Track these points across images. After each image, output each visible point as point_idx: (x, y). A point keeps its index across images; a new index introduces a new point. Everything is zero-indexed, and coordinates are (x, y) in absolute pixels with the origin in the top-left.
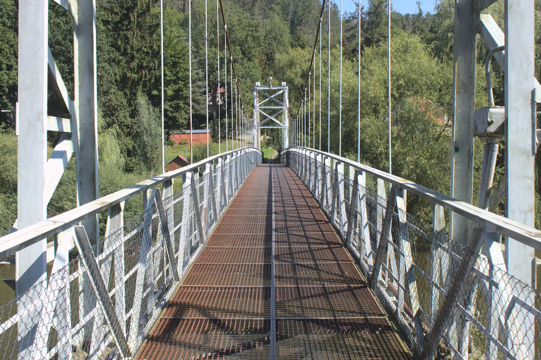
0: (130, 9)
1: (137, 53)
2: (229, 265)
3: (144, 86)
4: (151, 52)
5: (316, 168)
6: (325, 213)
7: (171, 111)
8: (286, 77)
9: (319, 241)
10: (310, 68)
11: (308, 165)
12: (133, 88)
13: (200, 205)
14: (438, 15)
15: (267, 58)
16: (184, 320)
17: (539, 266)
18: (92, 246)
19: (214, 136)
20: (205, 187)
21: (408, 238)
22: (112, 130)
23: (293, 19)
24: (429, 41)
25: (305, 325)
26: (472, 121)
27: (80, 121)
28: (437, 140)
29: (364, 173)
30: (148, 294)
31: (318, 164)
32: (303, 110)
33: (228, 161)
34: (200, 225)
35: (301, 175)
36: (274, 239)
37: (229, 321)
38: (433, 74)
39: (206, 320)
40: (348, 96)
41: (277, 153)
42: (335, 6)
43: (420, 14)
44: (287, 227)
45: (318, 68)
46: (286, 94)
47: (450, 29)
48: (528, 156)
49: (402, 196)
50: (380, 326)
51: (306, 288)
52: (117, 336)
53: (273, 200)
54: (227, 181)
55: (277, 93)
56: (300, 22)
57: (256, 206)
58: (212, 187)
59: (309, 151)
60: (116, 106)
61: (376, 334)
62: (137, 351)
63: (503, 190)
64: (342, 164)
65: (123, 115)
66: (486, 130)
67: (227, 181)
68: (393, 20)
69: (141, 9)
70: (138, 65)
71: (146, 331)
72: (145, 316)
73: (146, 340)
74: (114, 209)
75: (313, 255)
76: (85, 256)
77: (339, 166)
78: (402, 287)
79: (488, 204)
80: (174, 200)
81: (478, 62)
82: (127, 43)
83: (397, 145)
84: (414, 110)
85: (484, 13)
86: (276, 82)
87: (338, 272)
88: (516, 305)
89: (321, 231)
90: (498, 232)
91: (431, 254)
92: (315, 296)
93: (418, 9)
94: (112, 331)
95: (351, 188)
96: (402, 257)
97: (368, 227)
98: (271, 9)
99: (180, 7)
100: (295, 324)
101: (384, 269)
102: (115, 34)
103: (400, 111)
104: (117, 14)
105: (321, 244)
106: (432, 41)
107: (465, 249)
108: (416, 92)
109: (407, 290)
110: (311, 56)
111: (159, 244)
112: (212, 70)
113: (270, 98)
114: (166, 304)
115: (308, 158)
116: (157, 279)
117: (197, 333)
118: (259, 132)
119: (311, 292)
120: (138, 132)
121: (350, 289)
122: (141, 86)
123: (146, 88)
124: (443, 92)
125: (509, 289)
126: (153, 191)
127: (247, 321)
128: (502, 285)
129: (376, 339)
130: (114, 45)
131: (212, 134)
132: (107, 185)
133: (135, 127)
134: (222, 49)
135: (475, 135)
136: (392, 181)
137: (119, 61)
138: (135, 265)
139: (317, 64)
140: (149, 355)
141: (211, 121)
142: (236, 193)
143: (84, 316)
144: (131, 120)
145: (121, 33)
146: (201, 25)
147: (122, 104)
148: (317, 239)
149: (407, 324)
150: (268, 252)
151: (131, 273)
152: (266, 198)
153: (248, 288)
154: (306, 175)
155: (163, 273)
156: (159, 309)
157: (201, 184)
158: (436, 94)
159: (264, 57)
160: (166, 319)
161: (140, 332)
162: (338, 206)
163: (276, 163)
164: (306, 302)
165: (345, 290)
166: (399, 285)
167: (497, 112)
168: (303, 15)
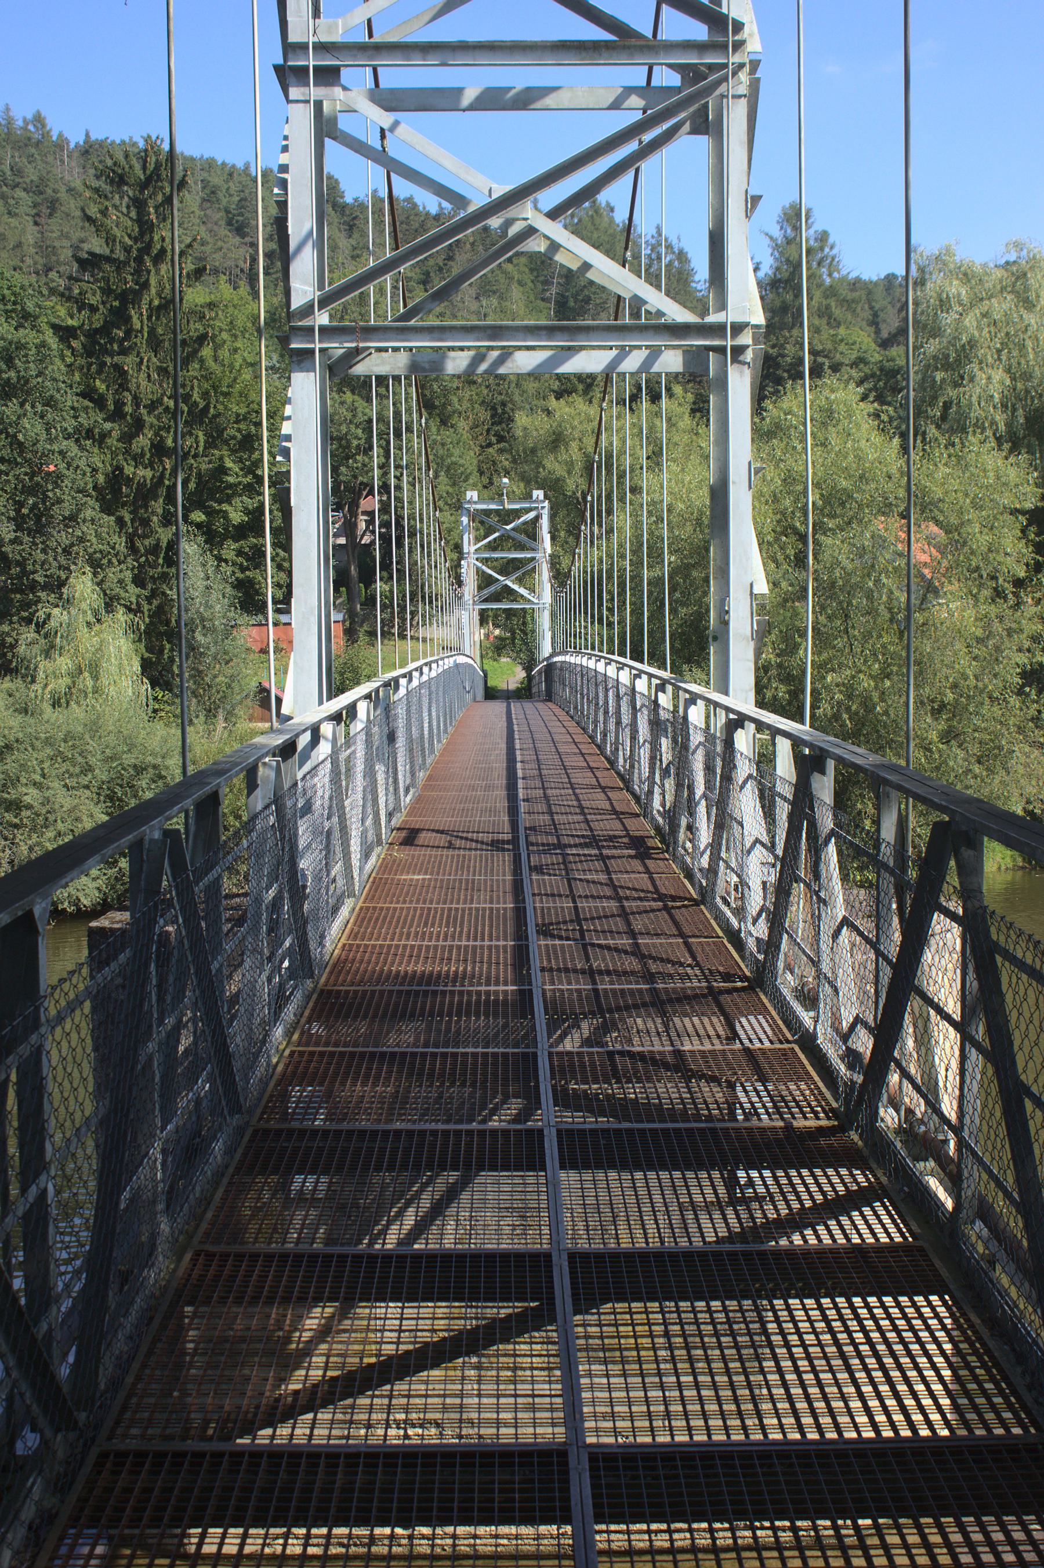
0: (129, 298)
1: (149, 413)
4: (186, 409)
5: (635, 710)
8: (543, 473)
12: (141, 507)
15: (492, 417)
20: (358, 755)
23: (563, 296)
41: (523, 674)
46: (545, 523)
55: (522, 520)
59: (627, 669)
60: (98, 555)
82: (124, 387)
86: (519, 488)
99: (241, 264)
102: (91, 364)
104: (93, 309)
113: (502, 532)
115: (600, 678)
118: (477, 618)
122: (161, 500)
131: (347, 624)
132: (120, 749)
137: (104, 435)
141: (343, 589)
144: (138, 590)
145: (108, 360)
147: (113, 548)
159: (484, 415)
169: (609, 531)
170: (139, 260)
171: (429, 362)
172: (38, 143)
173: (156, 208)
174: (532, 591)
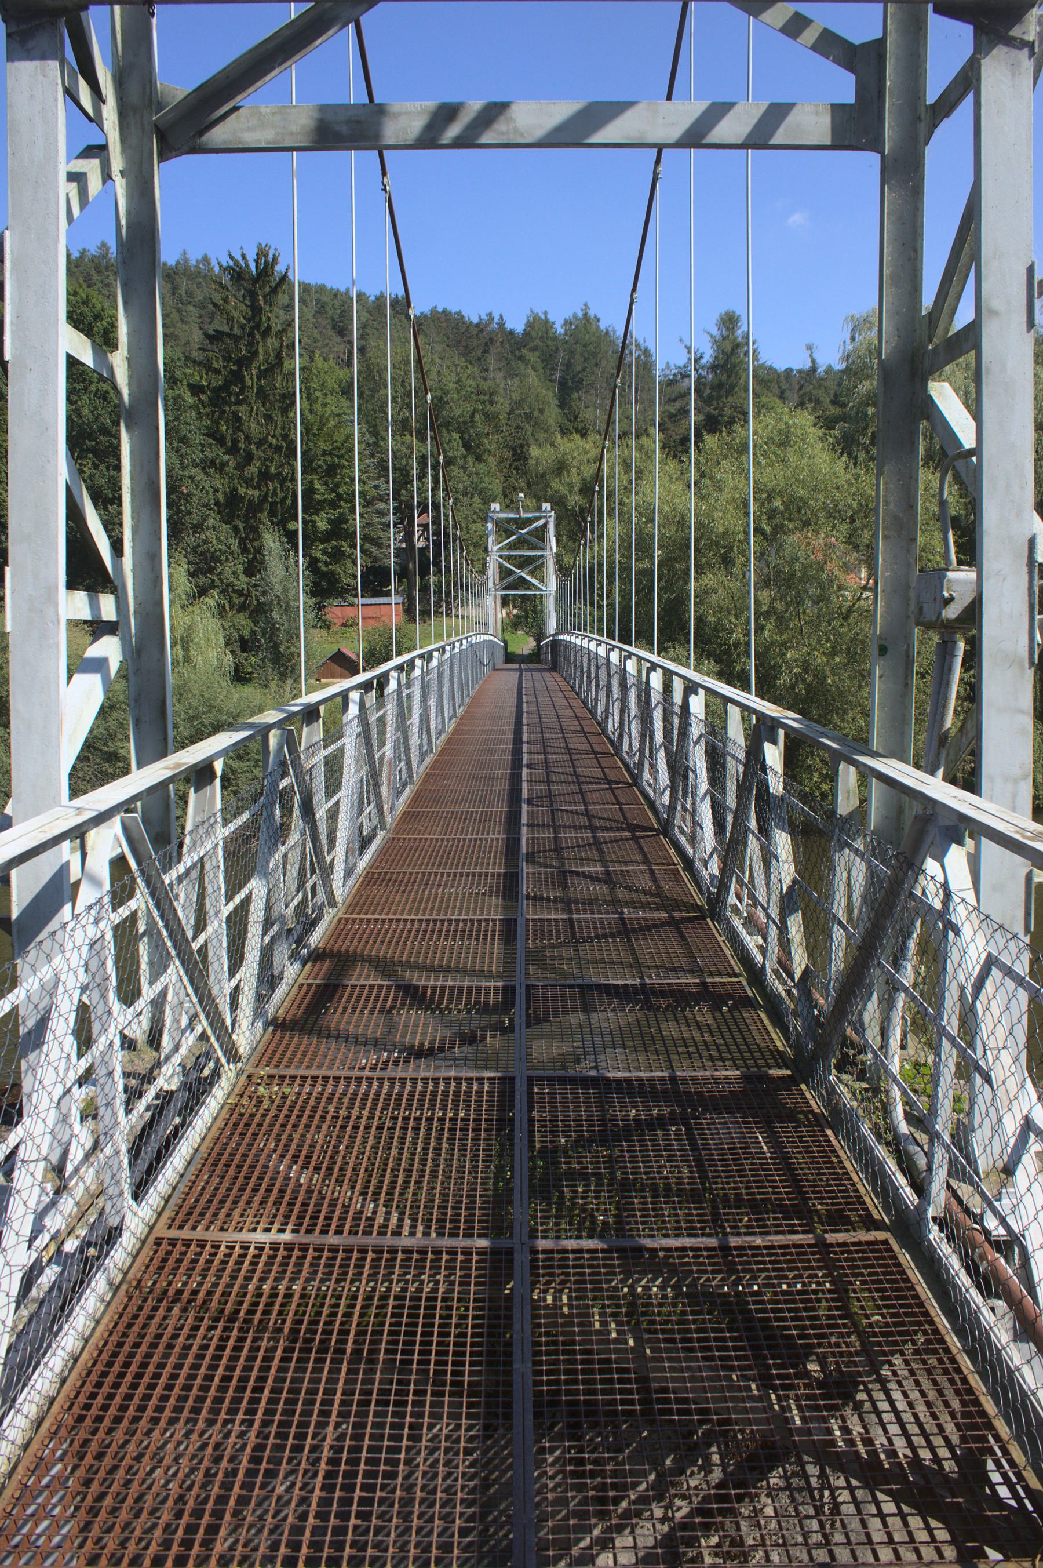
0: (244, 363)
2: (436, 874)
3: (272, 513)
5: (609, 676)
6: (626, 766)
7: (326, 562)
8: (550, 492)
9: (614, 825)
10: (598, 477)
11: (593, 670)
13: (377, 756)
14: (847, 371)
16: (346, 986)
17: (1040, 885)
18: (156, 853)
19: (409, 611)
20: (389, 718)
21: (786, 826)
22: (211, 600)
24: (828, 423)
25: (583, 996)
26: (912, 594)
27: (135, 597)
28: (846, 618)
29: (701, 691)
30: (273, 937)
31: (613, 669)
32: (585, 557)
33: (435, 663)
34: (378, 795)
35: (580, 687)
36: (524, 820)
37: (434, 988)
38: (838, 488)
39: (389, 988)
40: (671, 531)
42: (646, 352)
43: (814, 369)
44: (550, 796)
45: (612, 476)
46: (551, 527)
47: (870, 399)
48: (1022, 668)
49: (774, 742)
50: (730, 997)
51: (585, 919)
52: (211, 1024)
53: (525, 739)
54: (432, 702)
56: (578, 385)
57: (491, 752)
58: (403, 715)
61: (722, 1014)
62: (253, 1050)
63: (972, 734)
64: (660, 671)
65: (232, 570)
66: (940, 614)
67: (432, 702)
68: (759, 380)
69: (266, 361)
70: (260, 472)
71: (271, 1008)
72: (268, 979)
73: (271, 1028)
74: (201, 774)
75: (600, 851)
76: (142, 872)
77: (653, 675)
78: (774, 922)
79: (943, 761)
80: (325, 747)
81: (926, 465)
82: (239, 429)
83: (769, 627)
84: (802, 560)
85: (934, 380)
86: (531, 503)
87: (649, 886)
88: (995, 972)
89: (619, 803)
90: (962, 826)
91: (831, 860)
92: (605, 936)
93: (809, 360)
94: (202, 1016)
95: (676, 720)
96: (774, 861)
97: (708, 799)
98: (520, 358)
100: (563, 995)
101: (740, 882)
103: (774, 560)
104: (217, 372)
105: (618, 829)
106: (837, 422)
107: (896, 856)
108: (806, 524)
109: (783, 929)
110: (599, 451)
111: (294, 838)
112: (403, 480)
114: (310, 954)
116: (292, 906)
117: (372, 1012)
119: (595, 929)
120: (263, 603)
121: (672, 922)
123: (276, 516)
124: (858, 524)
125: (980, 941)
126: (282, 735)
127: (470, 988)
128: (967, 931)
129: (721, 1021)
130: (214, 434)
133: (254, 593)
134: (422, 439)
135: (917, 624)
136: (755, 711)
137: (223, 465)
138: (245, 884)
139: (612, 468)
140: (276, 1059)
142: (451, 727)
143: (151, 983)
144: (247, 579)
146: (382, 392)
148: (609, 820)
149: (783, 994)
150: (512, 845)
151: (238, 899)
152: (511, 736)
153: (472, 921)
154: (589, 690)
155: (305, 895)
156: (297, 966)
157: (381, 712)
158: (844, 527)
159: (507, 454)
160: (310, 985)
161: (258, 1012)
162: (651, 752)
163: (531, 662)
164: (586, 950)
165: (663, 925)
166: (768, 916)
167: (961, 578)
168: (584, 370)
169: (601, 536)
170: (251, 334)
171: (348, 122)
172: (205, 277)
173: (265, 297)
174: (541, 581)
